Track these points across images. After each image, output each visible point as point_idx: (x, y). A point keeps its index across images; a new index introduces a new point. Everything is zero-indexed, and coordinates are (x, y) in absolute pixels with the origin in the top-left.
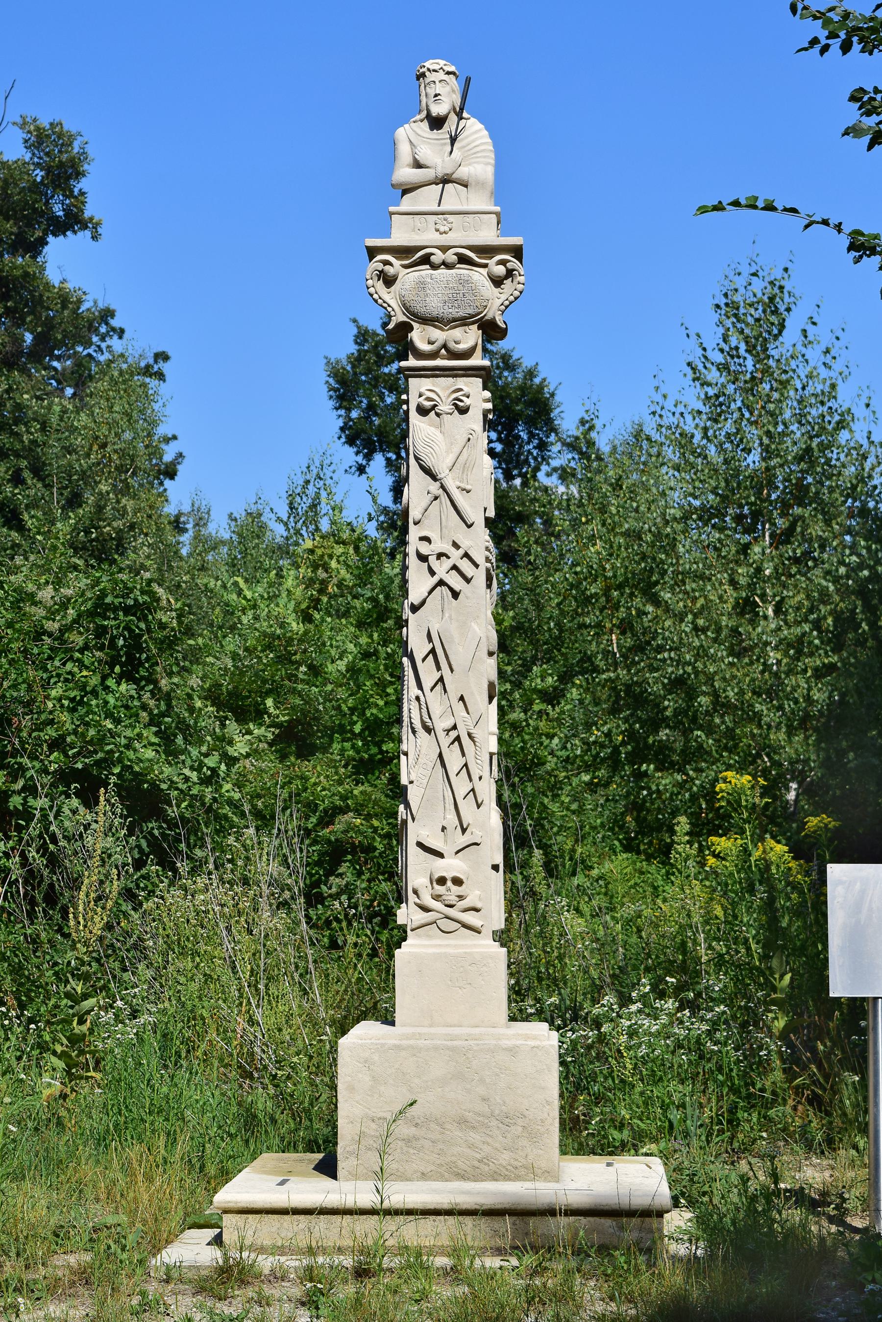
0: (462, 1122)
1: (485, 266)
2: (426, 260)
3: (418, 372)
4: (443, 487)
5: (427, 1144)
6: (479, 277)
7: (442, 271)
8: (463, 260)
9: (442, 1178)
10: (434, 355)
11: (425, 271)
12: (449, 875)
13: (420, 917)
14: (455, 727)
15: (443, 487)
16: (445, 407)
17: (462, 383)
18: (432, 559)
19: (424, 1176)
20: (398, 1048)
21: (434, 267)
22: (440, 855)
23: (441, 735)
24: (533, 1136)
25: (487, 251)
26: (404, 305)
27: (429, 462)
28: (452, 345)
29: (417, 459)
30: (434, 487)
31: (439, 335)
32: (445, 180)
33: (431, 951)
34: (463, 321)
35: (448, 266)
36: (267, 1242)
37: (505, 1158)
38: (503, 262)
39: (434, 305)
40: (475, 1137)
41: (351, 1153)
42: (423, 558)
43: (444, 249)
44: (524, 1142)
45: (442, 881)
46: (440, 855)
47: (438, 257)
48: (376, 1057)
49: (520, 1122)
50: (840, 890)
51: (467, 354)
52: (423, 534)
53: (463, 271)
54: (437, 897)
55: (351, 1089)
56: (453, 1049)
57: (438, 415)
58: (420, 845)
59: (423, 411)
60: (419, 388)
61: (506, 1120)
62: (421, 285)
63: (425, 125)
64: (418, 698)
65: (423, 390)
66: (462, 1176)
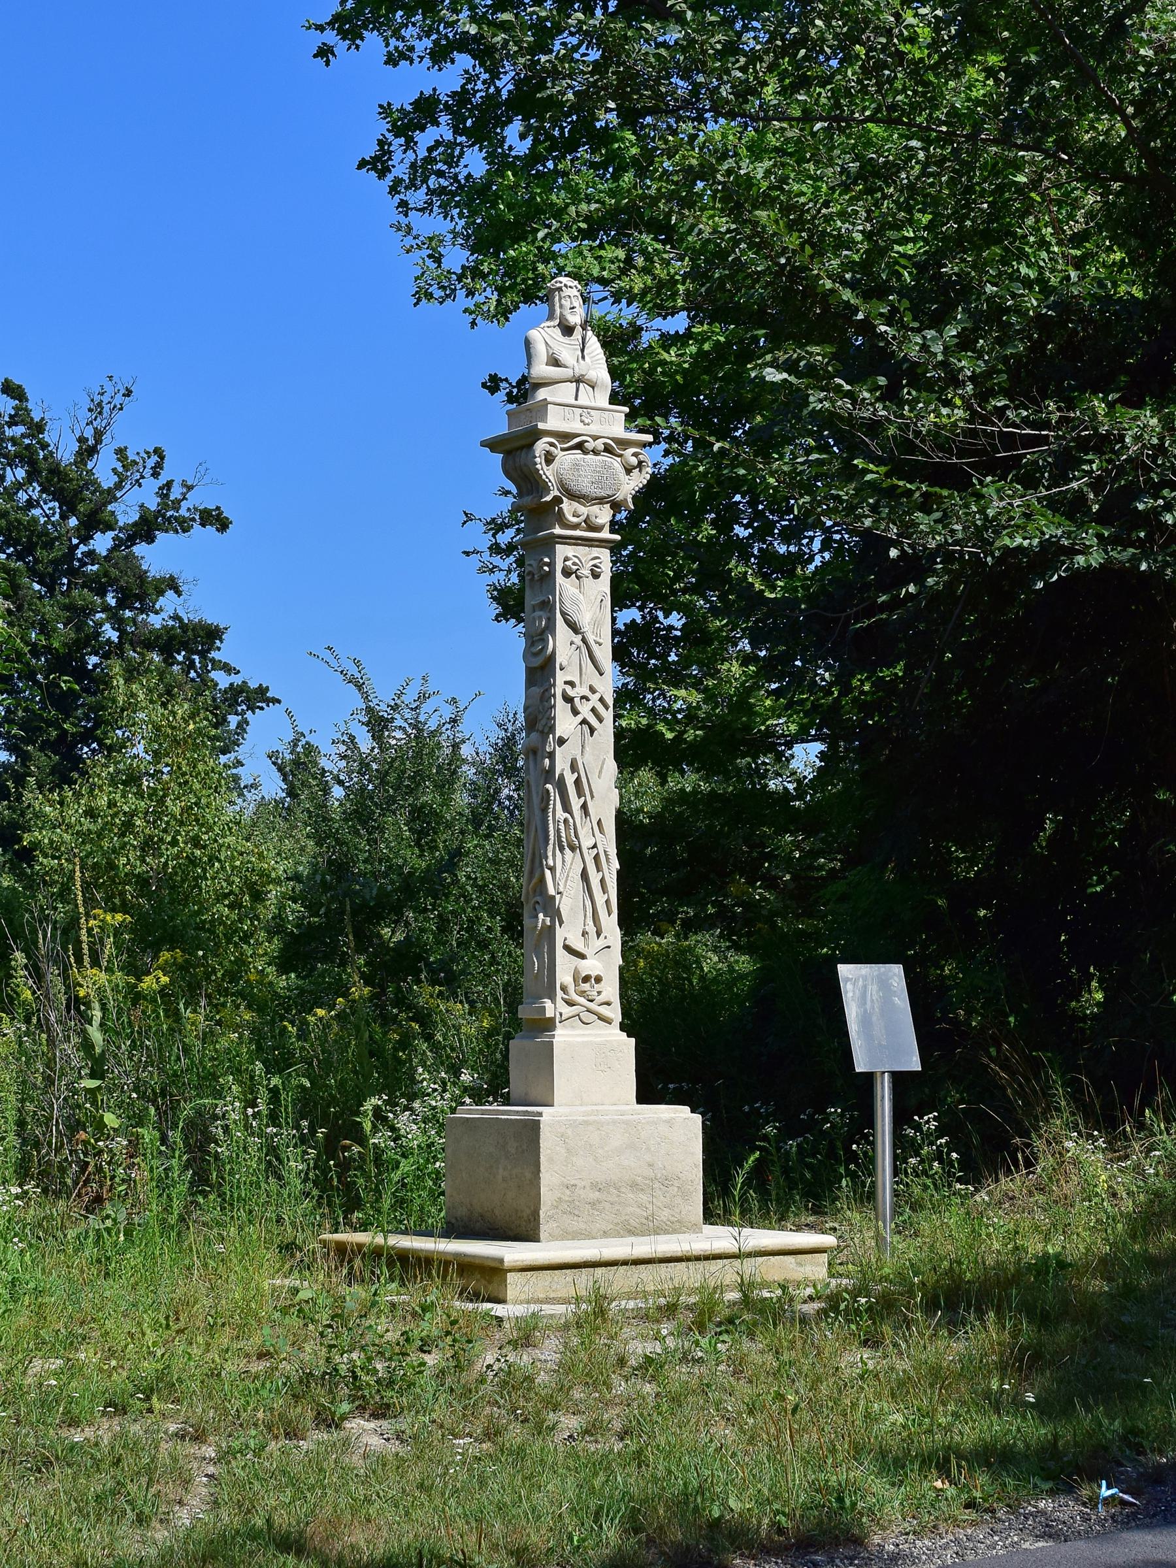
0: (634, 1186)
1: (620, 456)
2: (580, 446)
3: (565, 540)
4: (584, 640)
5: (607, 1206)
6: (616, 463)
7: (590, 456)
8: (608, 449)
9: (619, 1235)
10: (575, 527)
11: (577, 455)
12: (594, 974)
13: (567, 1011)
14: (595, 846)
15: (584, 640)
16: (585, 572)
17: (596, 552)
18: (577, 700)
19: (605, 1234)
20: (586, 1123)
21: (585, 452)
22: (582, 956)
23: (585, 851)
24: (686, 1195)
25: (624, 443)
26: (563, 486)
27: (575, 617)
28: (593, 519)
29: (563, 614)
30: (577, 639)
31: (583, 510)
32: (578, 380)
33: (579, 1039)
34: (601, 500)
35: (595, 452)
36: (541, 1296)
37: (665, 1215)
38: (635, 455)
39: (584, 485)
40: (644, 1198)
41: (551, 1217)
42: (568, 699)
43: (595, 438)
44: (678, 1200)
45: (586, 979)
46: (582, 956)
47: (590, 445)
48: (569, 1132)
49: (676, 1183)
50: (849, 986)
51: (598, 529)
52: (568, 678)
53: (605, 458)
54: (582, 994)
55: (551, 1160)
56: (626, 1123)
57: (578, 577)
58: (567, 948)
59: (567, 573)
60: (562, 551)
61: (666, 1182)
62: (576, 466)
63: (558, 331)
64: (566, 821)
65: (570, 555)
66: (632, 1233)
